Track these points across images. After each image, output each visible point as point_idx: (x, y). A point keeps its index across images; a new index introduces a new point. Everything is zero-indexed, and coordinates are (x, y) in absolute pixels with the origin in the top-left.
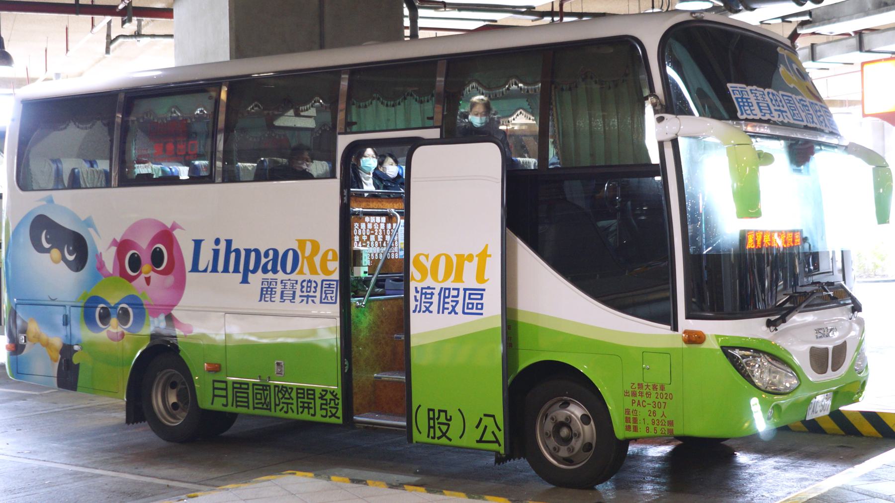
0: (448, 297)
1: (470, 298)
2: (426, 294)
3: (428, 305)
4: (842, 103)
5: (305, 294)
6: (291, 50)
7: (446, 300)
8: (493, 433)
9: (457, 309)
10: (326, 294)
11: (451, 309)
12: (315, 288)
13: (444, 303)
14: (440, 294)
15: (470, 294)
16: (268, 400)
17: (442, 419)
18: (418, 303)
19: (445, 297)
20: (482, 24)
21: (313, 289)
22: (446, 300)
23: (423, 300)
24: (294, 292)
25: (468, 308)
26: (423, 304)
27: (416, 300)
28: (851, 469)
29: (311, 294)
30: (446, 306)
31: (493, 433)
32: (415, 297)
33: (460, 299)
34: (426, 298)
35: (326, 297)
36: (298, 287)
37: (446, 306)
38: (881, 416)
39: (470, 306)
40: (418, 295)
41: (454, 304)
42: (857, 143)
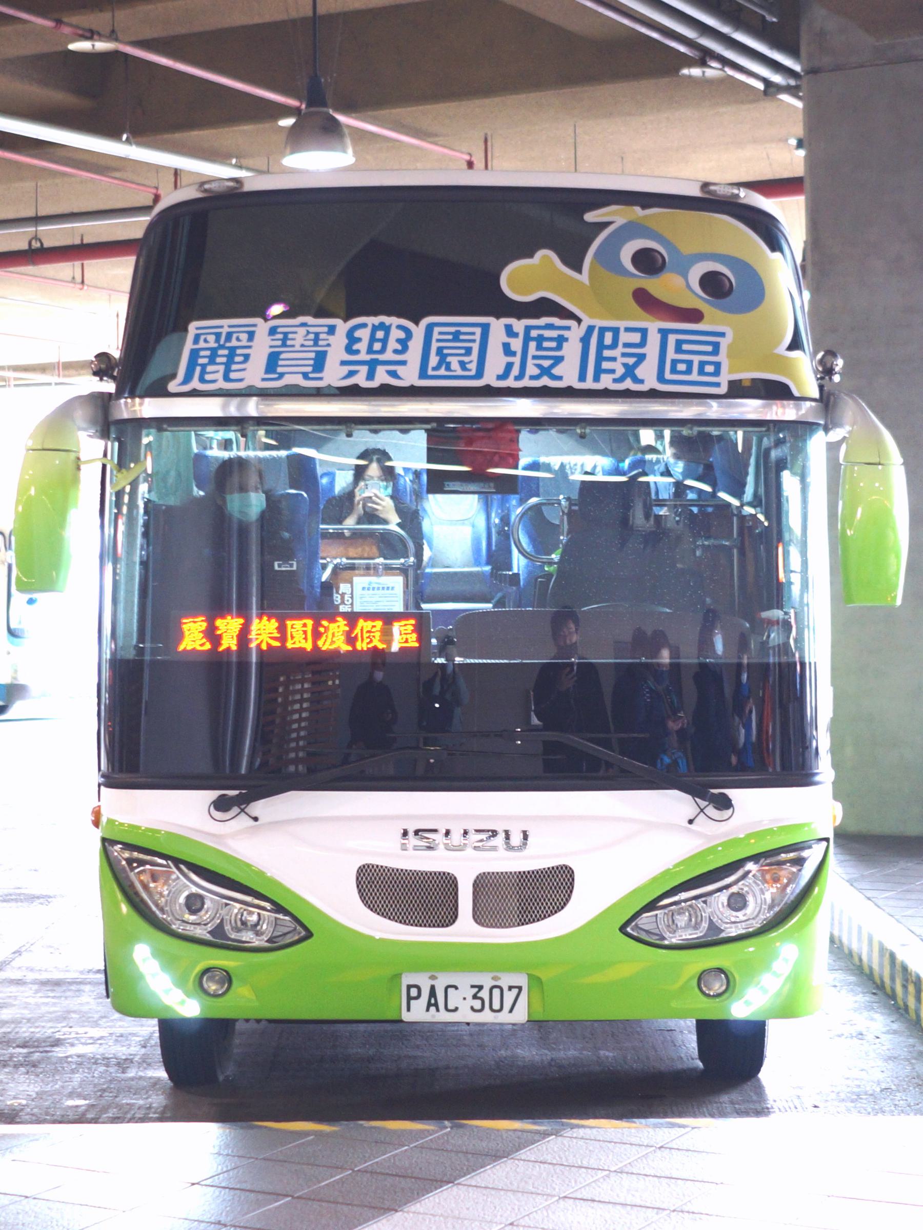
0: (614, 345)
1: (678, 350)
2: (540, 339)
4: (113, 16)
5: (363, 356)
7: (607, 353)
8: (511, 1011)
9: (639, 372)
11: (620, 371)
13: (600, 358)
14: (585, 341)
15: (679, 343)
16: (43, 1044)
17: (768, 877)
18: (517, 360)
19: (601, 346)
21: (392, 345)
22: (607, 353)
25: (674, 370)
26: (530, 362)
27: (507, 350)
29: (389, 355)
30: (605, 365)
31: (511, 1011)
34: (539, 347)
35: (443, 360)
37: (605, 365)
40: (516, 344)
41: (631, 361)
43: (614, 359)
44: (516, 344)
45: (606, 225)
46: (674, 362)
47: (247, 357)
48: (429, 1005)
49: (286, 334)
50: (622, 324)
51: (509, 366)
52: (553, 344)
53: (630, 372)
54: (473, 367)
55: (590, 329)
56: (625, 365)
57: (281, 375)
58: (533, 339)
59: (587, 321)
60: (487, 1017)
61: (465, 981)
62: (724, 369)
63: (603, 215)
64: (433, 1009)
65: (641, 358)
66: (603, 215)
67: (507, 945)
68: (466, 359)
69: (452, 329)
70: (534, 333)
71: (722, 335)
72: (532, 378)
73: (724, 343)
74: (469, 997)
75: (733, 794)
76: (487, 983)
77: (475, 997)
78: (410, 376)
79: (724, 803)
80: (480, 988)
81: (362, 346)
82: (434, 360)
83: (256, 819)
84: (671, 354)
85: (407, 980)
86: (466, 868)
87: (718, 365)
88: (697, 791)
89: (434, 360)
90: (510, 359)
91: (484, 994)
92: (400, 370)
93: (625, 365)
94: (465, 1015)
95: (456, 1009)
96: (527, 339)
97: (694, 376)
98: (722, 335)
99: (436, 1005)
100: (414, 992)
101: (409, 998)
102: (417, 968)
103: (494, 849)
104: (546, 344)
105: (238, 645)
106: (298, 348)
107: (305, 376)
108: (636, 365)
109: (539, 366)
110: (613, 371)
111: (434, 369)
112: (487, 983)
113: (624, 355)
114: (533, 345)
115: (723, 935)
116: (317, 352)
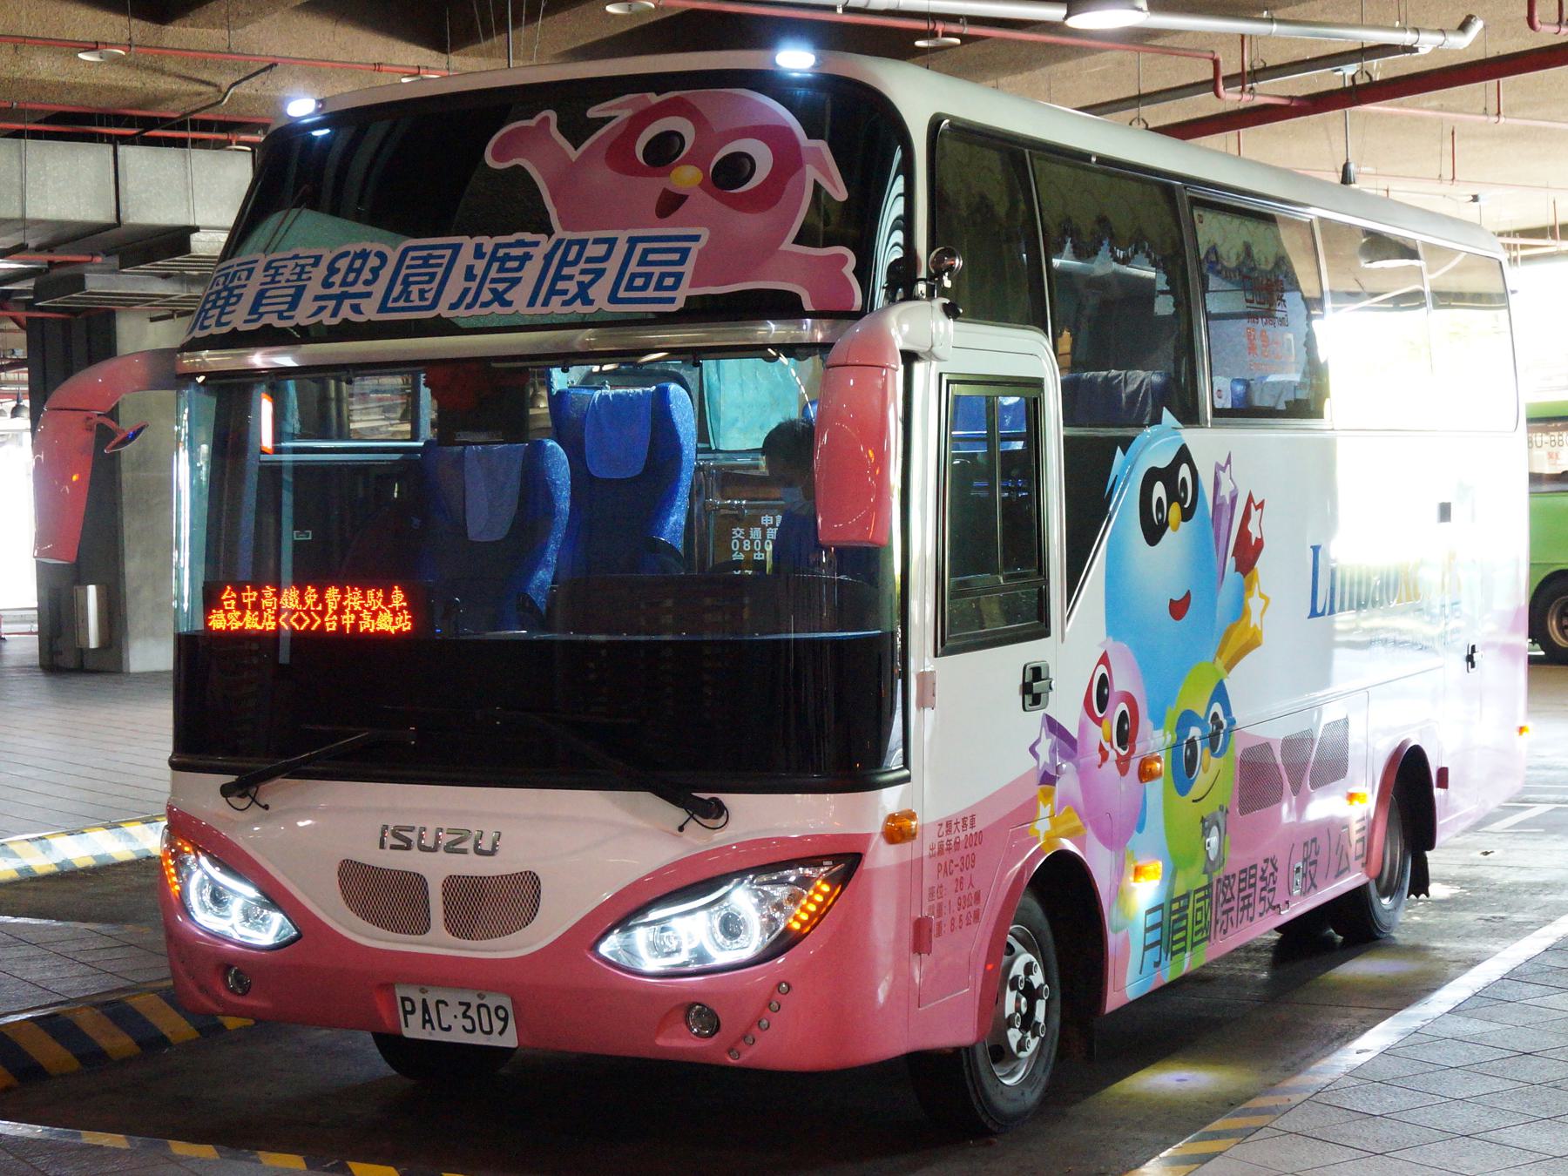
0: (575, 263)
1: (643, 262)
2: (508, 257)
3: (501, 287)
6: (739, 15)
9: (592, 293)
10: (406, 283)
12: (375, 272)
13: (559, 277)
14: (548, 258)
15: (646, 252)
18: (474, 285)
19: (564, 262)
20: (1217, 1125)
23: (493, 274)
24: (300, 290)
27: (470, 274)
28: (1516, 945)
32: (470, 269)
33: (612, 267)
35: (406, 294)
36: (320, 272)
38: (1536, 585)
39: (639, 282)
40: (480, 266)
41: (587, 278)
42: (457, 873)
43: (570, 278)
44: (480, 266)
45: (610, 119)
46: (634, 276)
47: (240, 296)
48: (425, 1022)
49: (277, 268)
50: (591, 235)
51: (466, 291)
52: (515, 264)
53: (583, 295)
54: (430, 295)
55: (559, 242)
56: (580, 284)
57: (261, 315)
58: (498, 259)
59: (559, 233)
60: (478, 1039)
61: (453, 997)
62: (686, 281)
63: (611, 108)
64: (428, 1026)
65: (599, 273)
66: (611, 108)
67: (534, 954)
68: (426, 287)
69: (424, 253)
70: (501, 253)
71: (696, 238)
72: (485, 305)
73: (695, 247)
74: (460, 1016)
75: (729, 799)
76: (475, 1002)
77: (465, 1016)
78: (370, 311)
79: (718, 810)
80: (468, 1005)
81: (337, 279)
82: (398, 289)
83: (266, 807)
84: (633, 267)
85: (400, 992)
86: (436, 869)
87: (679, 277)
88: (674, 794)
89: (398, 289)
90: (468, 284)
91: (473, 1013)
92: (364, 303)
93: (580, 284)
94: (458, 1036)
95: (449, 1029)
96: (493, 258)
97: (650, 293)
98: (696, 238)
99: (430, 1021)
100: (409, 1007)
101: (406, 1013)
102: (410, 981)
103: (464, 852)
104: (509, 265)
105: (548, 609)
106: (283, 284)
107: (281, 316)
108: (592, 282)
109: (493, 291)
110: (565, 292)
111: (396, 300)
112: (475, 1002)
113: (583, 272)
114: (496, 265)
115: (709, 965)
116: (297, 287)
